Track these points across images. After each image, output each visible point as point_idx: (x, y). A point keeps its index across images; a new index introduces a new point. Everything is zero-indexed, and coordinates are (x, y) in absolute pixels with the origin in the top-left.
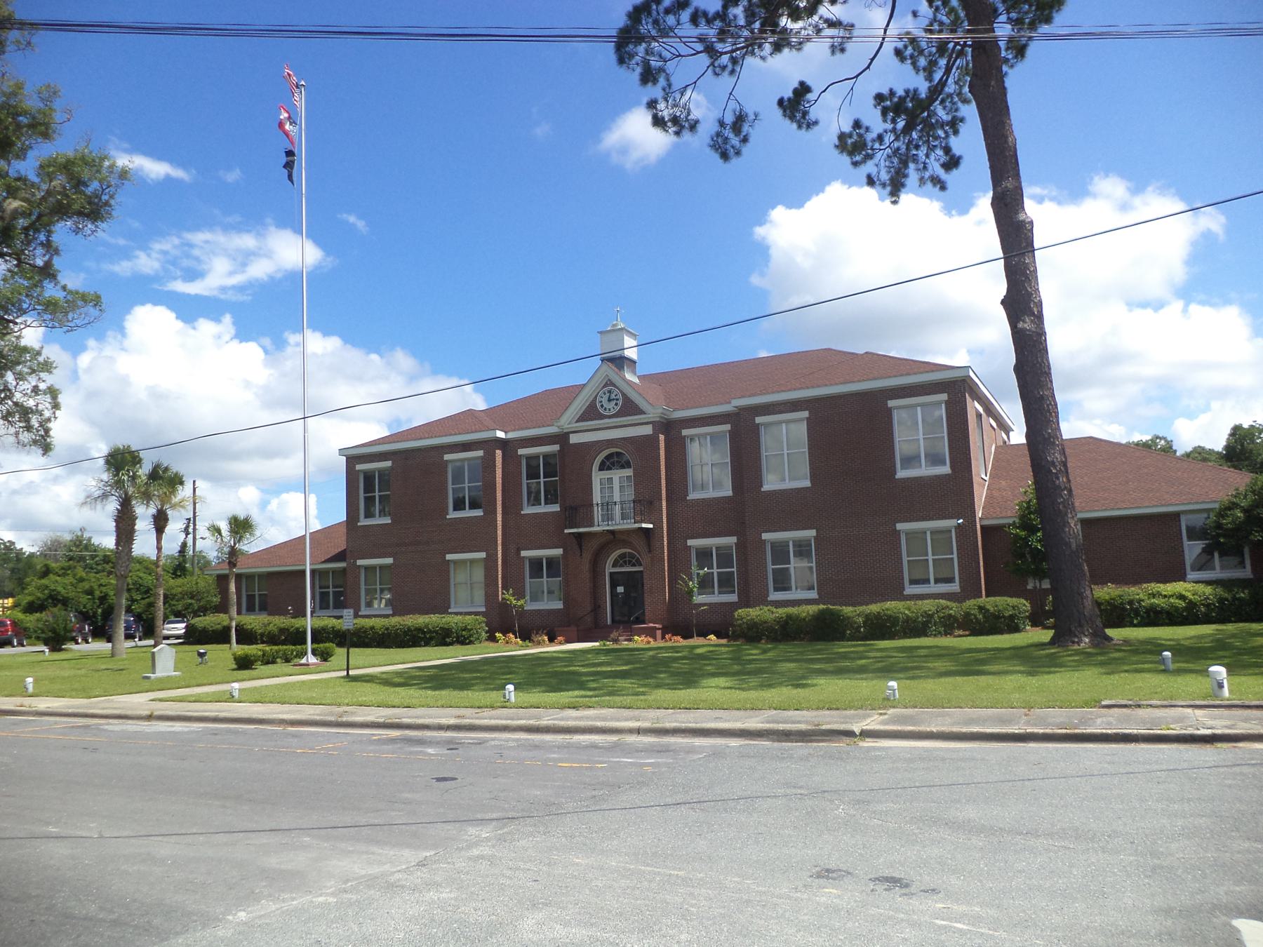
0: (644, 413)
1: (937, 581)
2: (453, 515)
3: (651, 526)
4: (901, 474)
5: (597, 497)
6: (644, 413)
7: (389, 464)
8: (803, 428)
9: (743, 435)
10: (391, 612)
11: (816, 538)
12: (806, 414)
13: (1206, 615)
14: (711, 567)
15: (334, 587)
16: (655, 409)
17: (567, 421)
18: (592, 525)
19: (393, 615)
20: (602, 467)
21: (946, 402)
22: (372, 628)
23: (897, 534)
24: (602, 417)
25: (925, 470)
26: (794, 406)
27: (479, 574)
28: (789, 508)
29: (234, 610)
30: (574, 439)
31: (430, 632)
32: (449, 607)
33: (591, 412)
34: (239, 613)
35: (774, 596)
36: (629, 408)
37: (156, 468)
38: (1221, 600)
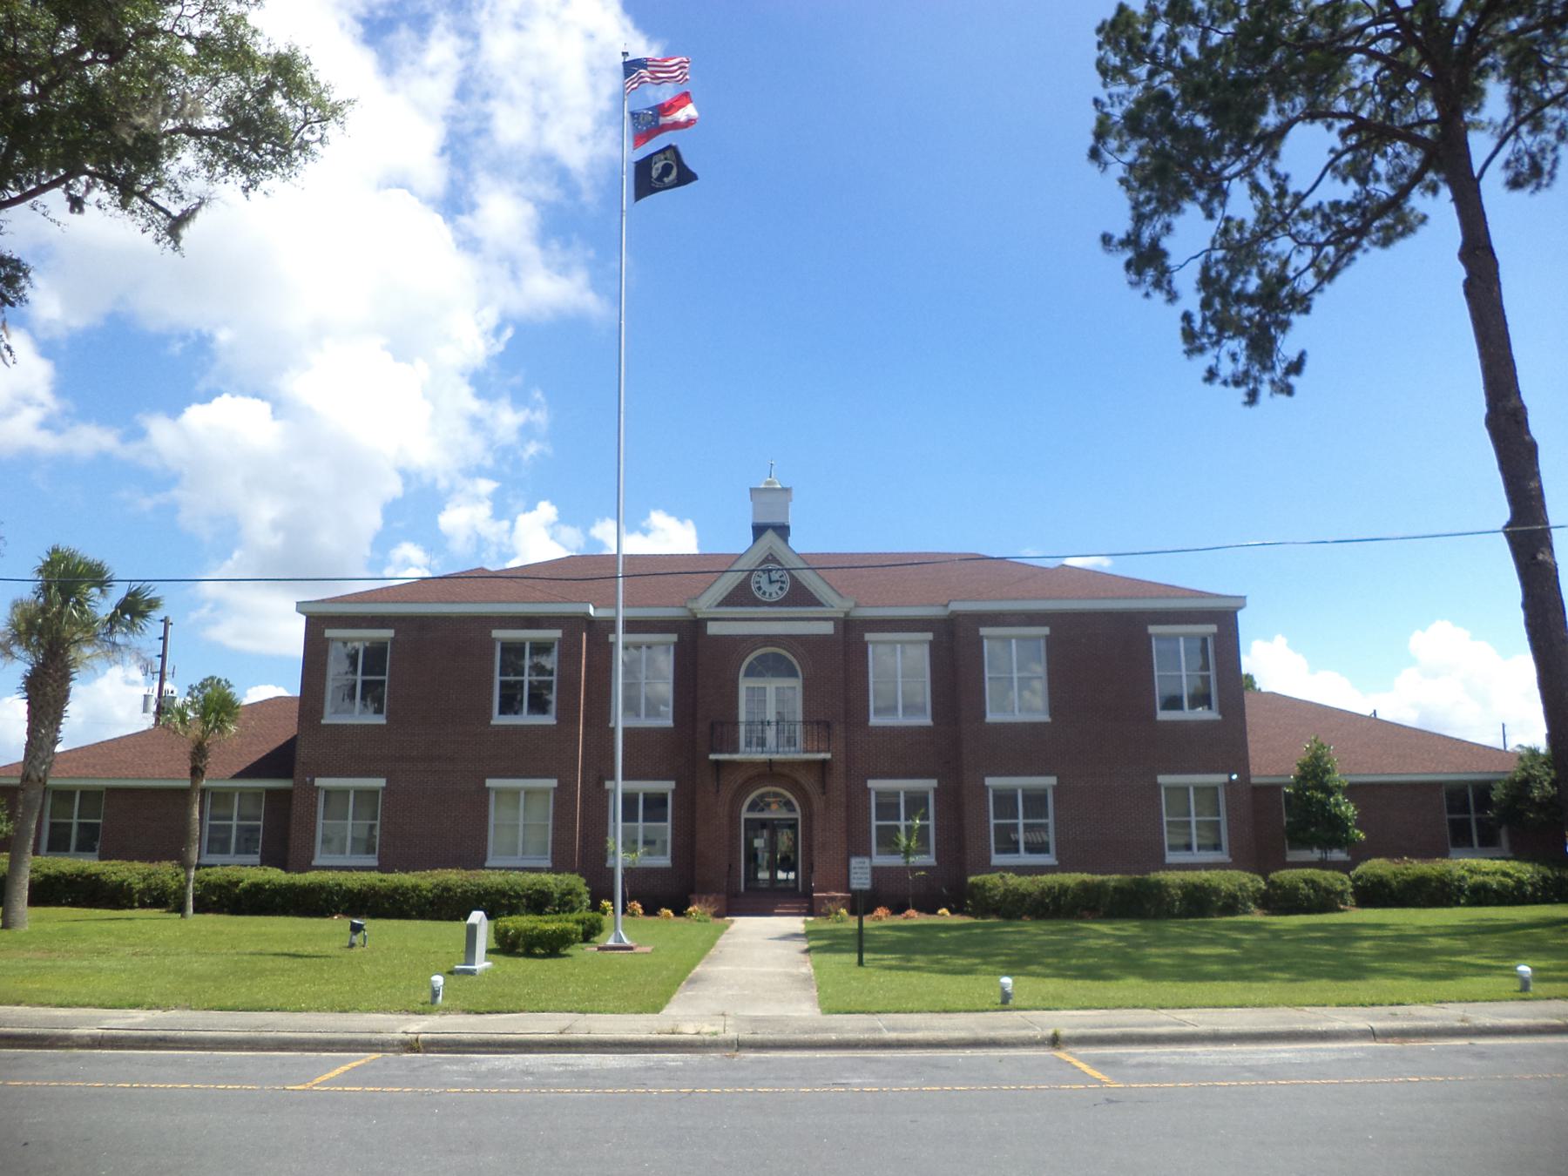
0: (819, 604)
1: (1199, 848)
2: (498, 720)
3: (828, 756)
4: (874, 721)
5: (742, 717)
6: (819, 604)
7: (388, 633)
8: (926, 649)
9: (955, 649)
10: (375, 863)
11: (1056, 789)
12: (929, 636)
13: (1533, 895)
14: (925, 817)
15: (241, 818)
16: (838, 605)
17: (705, 605)
18: (736, 750)
19: (549, 871)
20: (750, 673)
21: (931, 643)
22: (415, 888)
23: (1157, 786)
24: (757, 603)
25: (899, 720)
26: (1031, 619)
27: (543, 814)
28: (1021, 748)
29: (902, 828)
30: (713, 629)
31: (518, 896)
32: (485, 859)
33: (741, 596)
34: (36, 852)
35: (997, 859)
36: (799, 596)
37: (133, 595)
38: (1545, 879)
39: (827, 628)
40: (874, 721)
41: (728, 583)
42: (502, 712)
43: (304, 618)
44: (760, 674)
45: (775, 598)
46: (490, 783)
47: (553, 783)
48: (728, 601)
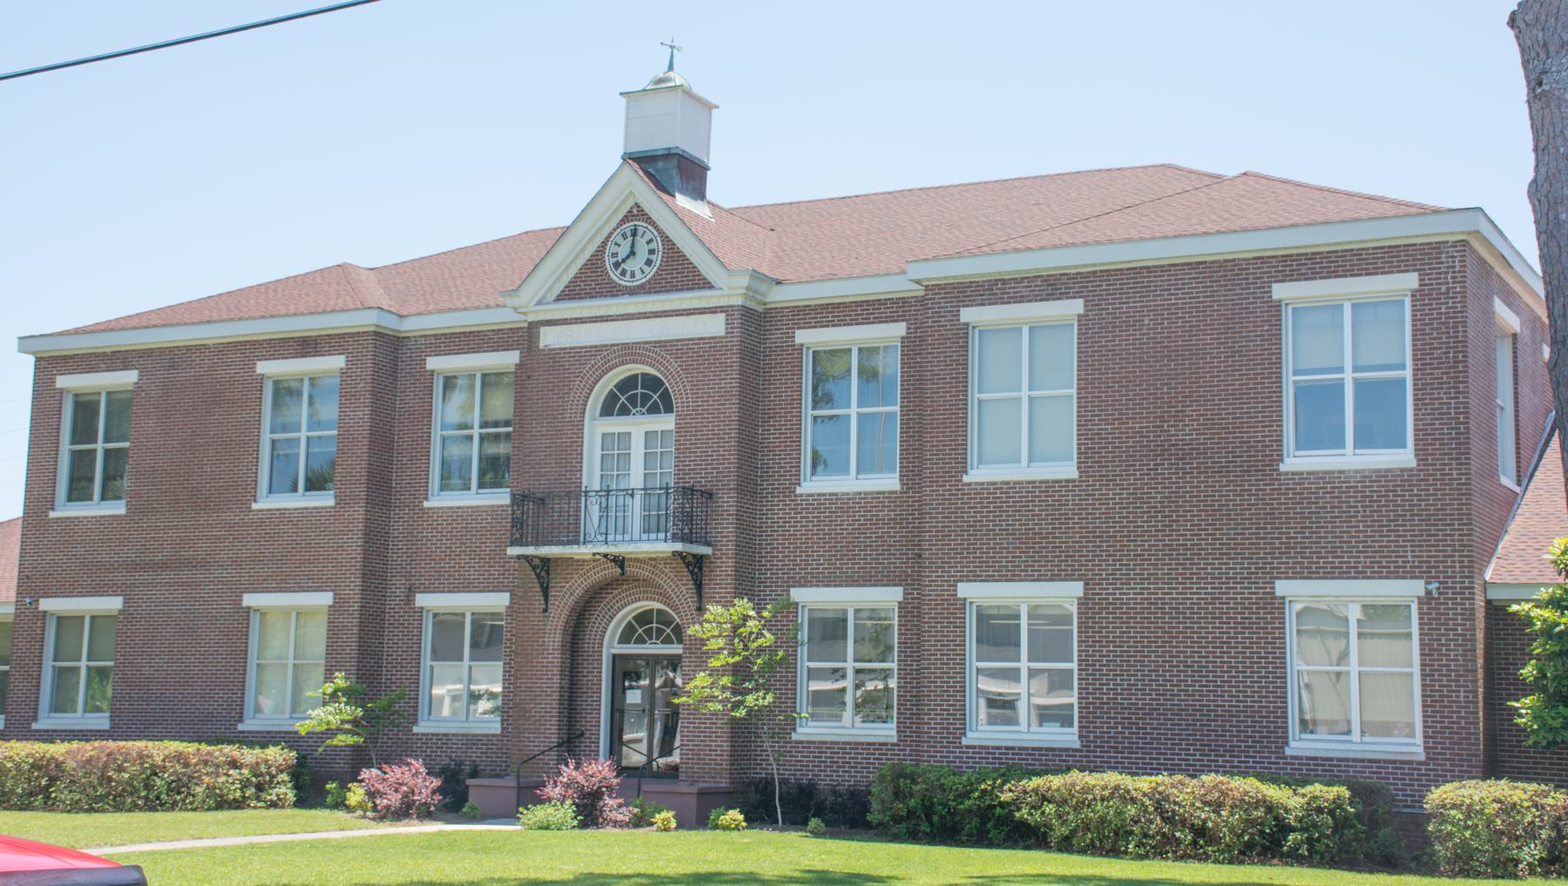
0: (707, 285)
6: (707, 285)
20: (610, 407)
24: (614, 291)
26: (1051, 286)
28: (1027, 531)
33: (592, 280)
39: (715, 326)
40: (1296, 461)
41: (563, 265)
42: (1304, 443)
43: (31, 360)
44: (624, 411)
45: (640, 280)
46: (249, 600)
47: (326, 599)
48: (571, 293)
